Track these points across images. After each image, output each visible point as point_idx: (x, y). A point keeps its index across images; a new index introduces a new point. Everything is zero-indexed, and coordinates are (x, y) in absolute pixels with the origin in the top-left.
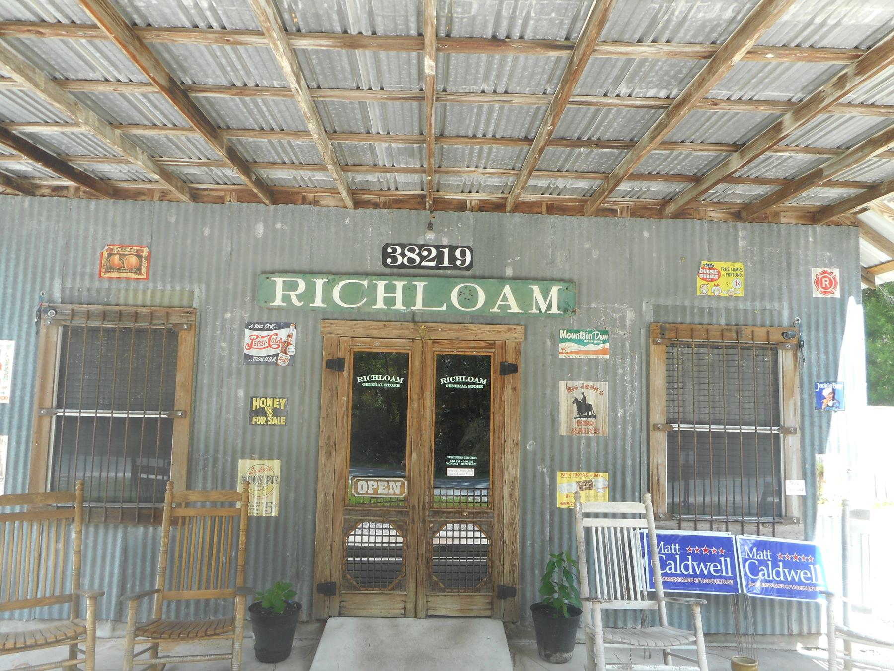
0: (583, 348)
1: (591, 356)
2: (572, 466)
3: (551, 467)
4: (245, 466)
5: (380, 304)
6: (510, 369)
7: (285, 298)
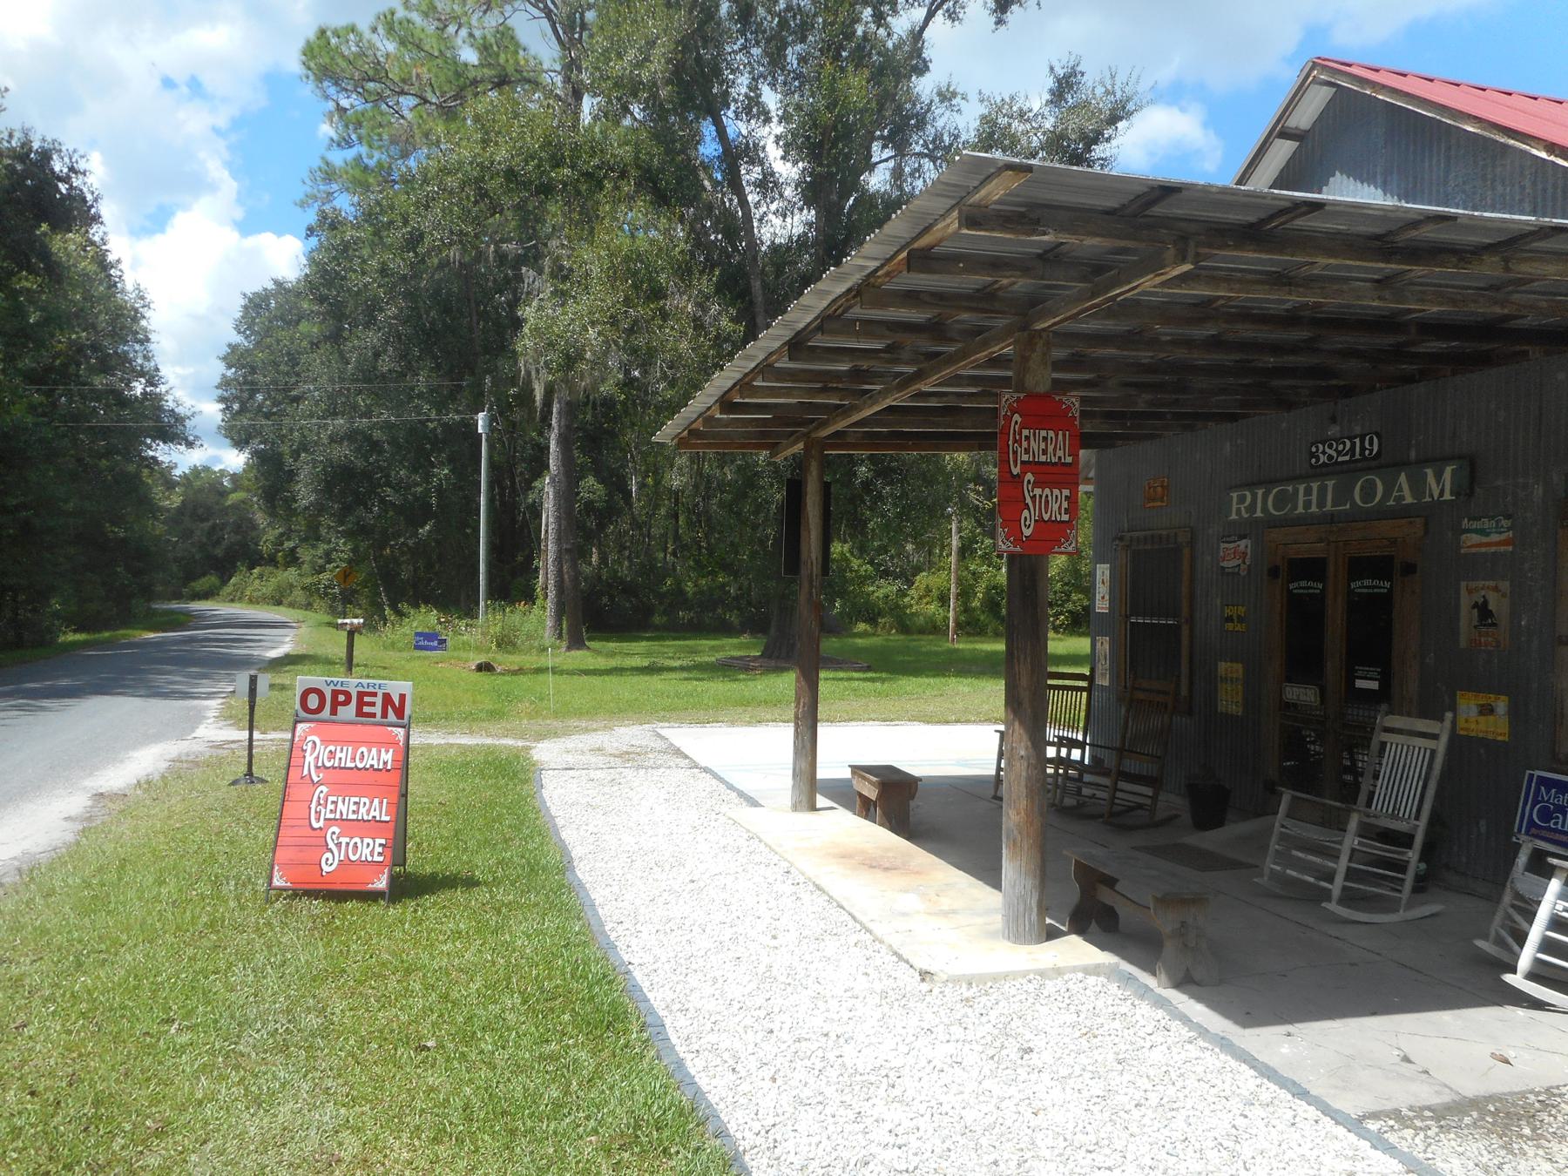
0: (1485, 540)
1: (1493, 549)
2: (1473, 686)
3: (521, 669)
4: (1223, 667)
5: (1300, 510)
6: (1409, 569)
7: (1238, 511)
